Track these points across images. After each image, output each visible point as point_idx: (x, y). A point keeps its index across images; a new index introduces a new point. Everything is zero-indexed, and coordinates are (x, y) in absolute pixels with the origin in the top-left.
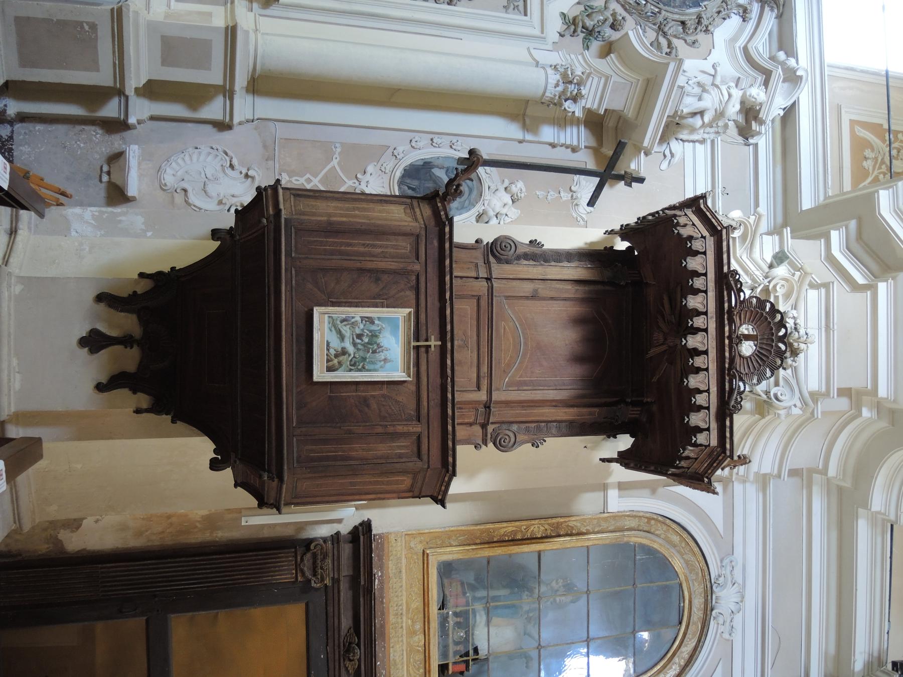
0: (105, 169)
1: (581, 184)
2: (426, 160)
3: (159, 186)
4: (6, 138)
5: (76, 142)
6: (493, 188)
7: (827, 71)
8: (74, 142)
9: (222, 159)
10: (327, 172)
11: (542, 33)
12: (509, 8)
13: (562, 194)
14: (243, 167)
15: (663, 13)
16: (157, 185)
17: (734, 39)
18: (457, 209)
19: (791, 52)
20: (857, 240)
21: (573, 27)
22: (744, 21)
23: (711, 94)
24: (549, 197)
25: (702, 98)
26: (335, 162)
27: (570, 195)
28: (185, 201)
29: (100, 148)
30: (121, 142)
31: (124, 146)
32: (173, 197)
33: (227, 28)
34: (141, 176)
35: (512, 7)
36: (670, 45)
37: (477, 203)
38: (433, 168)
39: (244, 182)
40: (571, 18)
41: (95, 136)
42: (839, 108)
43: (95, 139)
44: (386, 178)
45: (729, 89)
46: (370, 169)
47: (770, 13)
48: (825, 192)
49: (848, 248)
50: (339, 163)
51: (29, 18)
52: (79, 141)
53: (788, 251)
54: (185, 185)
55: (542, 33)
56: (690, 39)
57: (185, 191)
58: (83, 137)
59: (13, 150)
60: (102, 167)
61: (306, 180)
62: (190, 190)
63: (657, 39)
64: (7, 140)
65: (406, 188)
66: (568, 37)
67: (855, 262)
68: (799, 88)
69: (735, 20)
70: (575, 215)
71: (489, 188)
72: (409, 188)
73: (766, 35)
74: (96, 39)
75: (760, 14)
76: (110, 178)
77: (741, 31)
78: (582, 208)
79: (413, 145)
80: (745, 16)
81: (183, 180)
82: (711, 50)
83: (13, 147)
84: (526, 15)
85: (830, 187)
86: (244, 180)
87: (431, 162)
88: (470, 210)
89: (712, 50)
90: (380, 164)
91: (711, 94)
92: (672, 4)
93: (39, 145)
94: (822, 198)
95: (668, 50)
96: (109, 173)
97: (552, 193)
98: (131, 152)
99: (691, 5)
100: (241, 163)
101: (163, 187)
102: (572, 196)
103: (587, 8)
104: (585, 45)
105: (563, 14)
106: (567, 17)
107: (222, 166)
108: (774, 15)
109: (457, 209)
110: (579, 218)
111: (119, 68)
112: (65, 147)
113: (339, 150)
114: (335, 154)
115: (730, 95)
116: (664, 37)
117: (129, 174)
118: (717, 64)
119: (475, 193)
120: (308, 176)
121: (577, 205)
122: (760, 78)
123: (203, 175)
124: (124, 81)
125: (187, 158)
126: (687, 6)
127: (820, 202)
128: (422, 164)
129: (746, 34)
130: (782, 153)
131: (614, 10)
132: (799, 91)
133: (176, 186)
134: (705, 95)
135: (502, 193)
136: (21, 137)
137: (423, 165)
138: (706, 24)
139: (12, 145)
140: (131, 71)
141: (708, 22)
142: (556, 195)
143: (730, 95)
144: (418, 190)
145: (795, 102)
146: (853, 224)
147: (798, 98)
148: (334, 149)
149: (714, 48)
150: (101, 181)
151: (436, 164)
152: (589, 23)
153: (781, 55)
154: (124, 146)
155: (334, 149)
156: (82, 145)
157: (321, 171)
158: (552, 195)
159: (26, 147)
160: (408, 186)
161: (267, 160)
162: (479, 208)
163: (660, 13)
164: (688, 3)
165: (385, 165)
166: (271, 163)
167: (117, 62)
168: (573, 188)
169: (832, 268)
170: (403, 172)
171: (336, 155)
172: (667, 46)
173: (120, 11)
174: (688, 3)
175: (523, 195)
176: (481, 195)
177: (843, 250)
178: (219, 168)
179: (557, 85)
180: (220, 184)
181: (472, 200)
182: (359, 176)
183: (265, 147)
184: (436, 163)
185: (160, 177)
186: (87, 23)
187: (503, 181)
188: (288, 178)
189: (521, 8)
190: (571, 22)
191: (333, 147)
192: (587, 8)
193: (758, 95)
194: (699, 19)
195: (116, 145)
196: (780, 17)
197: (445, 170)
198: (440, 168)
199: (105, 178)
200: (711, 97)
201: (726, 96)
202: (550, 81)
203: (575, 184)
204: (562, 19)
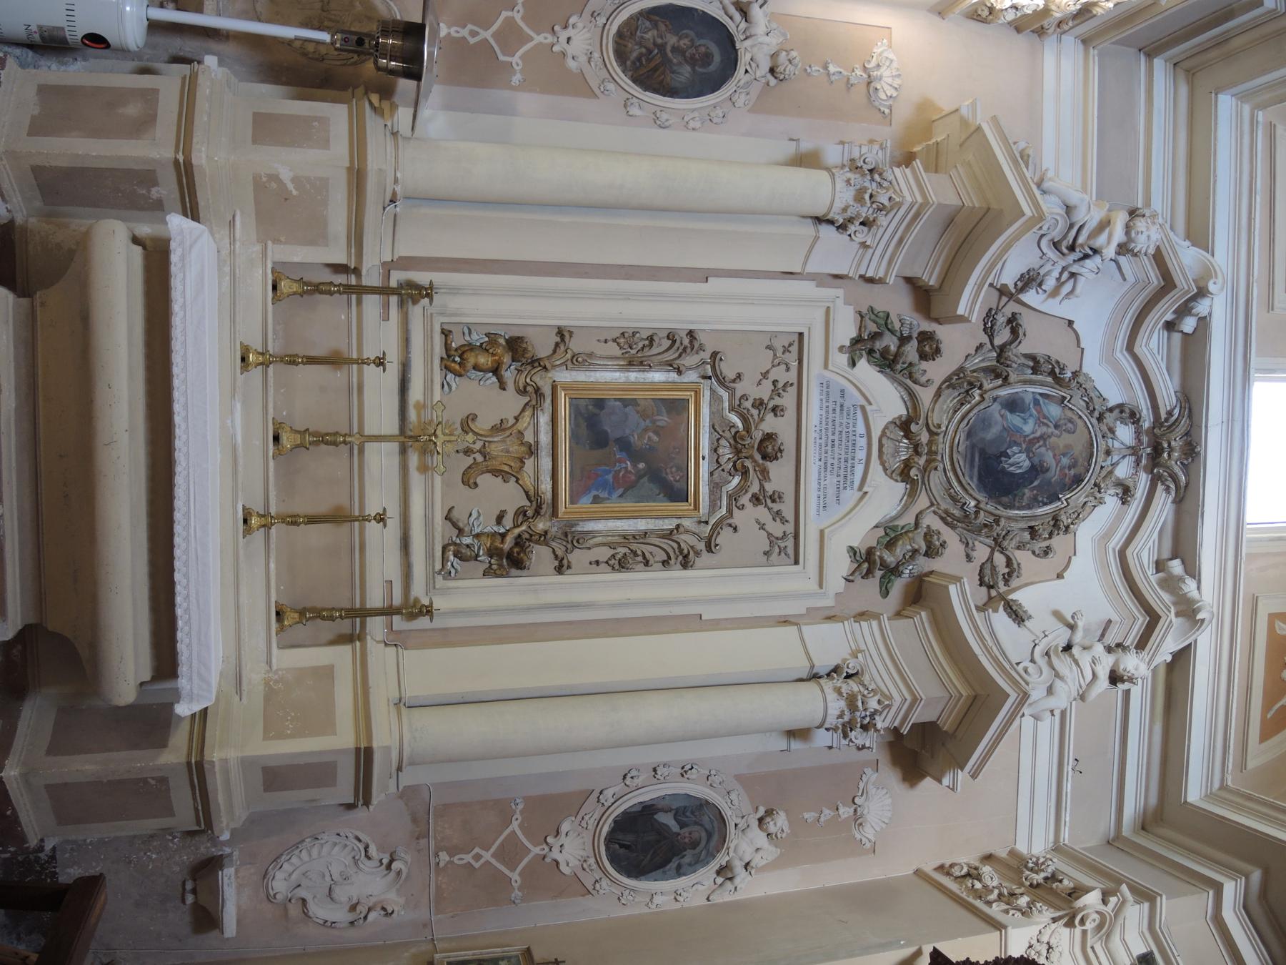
0: (189, 886)
1: (870, 793)
2: (646, 804)
3: (265, 898)
4: (46, 858)
5: (145, 854)
6: (742, 824)
7: (1247, 536)
8: (142, 854)
9: (353, 848)
10: (503, 841)
11: (821, 586)
12: (771, 554)
13: (842, 810)
14: (384, 853)
15: (1003, 522)
16: (263, 895)
17: (1107, 535)
18: (690, 865)
19: (1192, 570)
20: (1259, 897)
21: (866, 565)
22: (1123, 503)
23: (1066, 682)
24: (822, 819)
25: (1053, 689)
26: (515, 825)
27: (852, 810)
28: (304, 911)
29: (181, 857)
30: (209, 845)
31: (213, 850)
32: (286, 910)
33: (358, 750)
34: (240, 888)
35: (777, 550)
36: (1009, 563)
37: (718, 852)
38: (656, 813)
39: (386, 875)
40: (863, 551)
41: (172, 841)
42: (1255, 601)
43: (171, 845)
44: (588, 837)
45: (1094, 663)
46: (565, 827)
47: (1164, 495)
48: (1223, 779)
49: (1245, 907)
50: (520, 826)
51: (66, 784)
52: (150, 851)
53: (1160, 928)
54: (302, 893)
55: (821, 586)
56: (1040, 545)
57: (304, 901)
58: (155, 844)
59: (57, 874)
60: (184, 883)
61: (473, 857)
62: (309, 898)
63: (990, 559)
64: (47, 862)
65: (617, 846)
66: (857, 577)
67: (1255, 941)
68: (1198, 630)
69: (1111, 502)
70: (858, 836)
71: (736, 825)
72: (622, 846)
73: (1156, 535)
74: (168, 790)
75: (1148, 492)
76: (196, 898)
77: (1119, 519)
78: (869, 826)
79: (627, 783)
80: (1126, 499)
81: (299, 886)
82: (1070, 558)
83: (57, 870)
84: (796, 562)
85: (1230, 772)
86: (386, 872)
87: (653, 805)
88: (708, 863)
89: (1073, 558)
90: (579, 817)
91: (1066, 682)
92: (1017, 504)
93: (94, 864)
94: (1217, 785)
95: (1007, 570)
96: (194, 891)
97: (826, 811)
98: (226, 879)
99: (1045, 500)
100: (381, 849)
101: (270, 898)
102: (855, 811)
103: (888, 531)
104: (884, 588)
105: (852, 548)
106: (858, 554)
107: (354, 858)
108: (1171, 499)
109: (690, 865)
110: (864, 839)
111: (199, 790)
112: (130, 862)
113: (521, 807)
114: (515, 812)
115: (1094, 675)
116: (1002, 553)
117: (225, 909)
118: (1079, 616)
119: (716, 837)
120: (477, 850)
121: (861, 824)
122: (1141, 619)
123: (328, 878)
124: (205, 783)
125: (304, 854)
126: (1039, 502)
127: (1214, 790)
128: (640, 809)
129: (1125, 525)
130: (1161, 764)
131: (928, 527)
132: (1198, 633)
133: (289, 896)
134: (1058, 684)
135: (756, 833)
136: (67, 855)
137: (642, 811)
138: (1065, 524)
139: (55, 867)
140: (215, 773)
141: (1070, 521)
142: (832, 814)
143: (1094, 675)
144: (634, 847)
145: (1190, 645)
146: (1256, 876)
147: (1196, 641)
148: (514, 807)
149: (1075, 554)
150: (183, 901)
151: (660, 807)
152: (890, 559)
153: (1176, 567)
154: (213, 850)
155: (514, 807)
156: (154, 856)
157: (494, 841)
158: (828, 813)
159: (76, 868)
160: (619, 844)
161: (418, 839)
162: (721, 859)
163: (997, 521)
164: (1040, 499)
165: (586, 818)
166: (423, 842)
167: (200, 808)
168: (857, 800)
169: (1221, 938)
170: (612, 825)
171: (518, 815)
172: (1005, 564)
173: (200, 766)
174: (1040, 499)
175: (784, 835)
176: (725, 841)
177: (1239, 909)
178: (349, 861)
179: (841, 716)
180: (352, 884)
181: (711, 849)
182: (556, 28)
183: (415, 820)
184: (661, 804)
185: (267, 884)
186: (153, 778)
187: (757, 808)
188: (447, 858)
189: (791, 551)
190: (864, 558)
191: (512, 804)
192: (888, 531)
193: (1136, 669)
194: (1056, 520)
195: (202, 849)
196: (1178, 501)
197: (673, 812)
198: (666, 812)
199: (190, 899)
200: (1066, 687)
201: (1089, 677)
202: (830, 711)
203: (860, 794)
204: (850, 557)
